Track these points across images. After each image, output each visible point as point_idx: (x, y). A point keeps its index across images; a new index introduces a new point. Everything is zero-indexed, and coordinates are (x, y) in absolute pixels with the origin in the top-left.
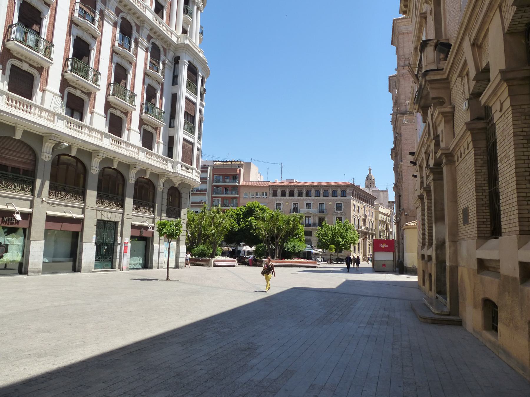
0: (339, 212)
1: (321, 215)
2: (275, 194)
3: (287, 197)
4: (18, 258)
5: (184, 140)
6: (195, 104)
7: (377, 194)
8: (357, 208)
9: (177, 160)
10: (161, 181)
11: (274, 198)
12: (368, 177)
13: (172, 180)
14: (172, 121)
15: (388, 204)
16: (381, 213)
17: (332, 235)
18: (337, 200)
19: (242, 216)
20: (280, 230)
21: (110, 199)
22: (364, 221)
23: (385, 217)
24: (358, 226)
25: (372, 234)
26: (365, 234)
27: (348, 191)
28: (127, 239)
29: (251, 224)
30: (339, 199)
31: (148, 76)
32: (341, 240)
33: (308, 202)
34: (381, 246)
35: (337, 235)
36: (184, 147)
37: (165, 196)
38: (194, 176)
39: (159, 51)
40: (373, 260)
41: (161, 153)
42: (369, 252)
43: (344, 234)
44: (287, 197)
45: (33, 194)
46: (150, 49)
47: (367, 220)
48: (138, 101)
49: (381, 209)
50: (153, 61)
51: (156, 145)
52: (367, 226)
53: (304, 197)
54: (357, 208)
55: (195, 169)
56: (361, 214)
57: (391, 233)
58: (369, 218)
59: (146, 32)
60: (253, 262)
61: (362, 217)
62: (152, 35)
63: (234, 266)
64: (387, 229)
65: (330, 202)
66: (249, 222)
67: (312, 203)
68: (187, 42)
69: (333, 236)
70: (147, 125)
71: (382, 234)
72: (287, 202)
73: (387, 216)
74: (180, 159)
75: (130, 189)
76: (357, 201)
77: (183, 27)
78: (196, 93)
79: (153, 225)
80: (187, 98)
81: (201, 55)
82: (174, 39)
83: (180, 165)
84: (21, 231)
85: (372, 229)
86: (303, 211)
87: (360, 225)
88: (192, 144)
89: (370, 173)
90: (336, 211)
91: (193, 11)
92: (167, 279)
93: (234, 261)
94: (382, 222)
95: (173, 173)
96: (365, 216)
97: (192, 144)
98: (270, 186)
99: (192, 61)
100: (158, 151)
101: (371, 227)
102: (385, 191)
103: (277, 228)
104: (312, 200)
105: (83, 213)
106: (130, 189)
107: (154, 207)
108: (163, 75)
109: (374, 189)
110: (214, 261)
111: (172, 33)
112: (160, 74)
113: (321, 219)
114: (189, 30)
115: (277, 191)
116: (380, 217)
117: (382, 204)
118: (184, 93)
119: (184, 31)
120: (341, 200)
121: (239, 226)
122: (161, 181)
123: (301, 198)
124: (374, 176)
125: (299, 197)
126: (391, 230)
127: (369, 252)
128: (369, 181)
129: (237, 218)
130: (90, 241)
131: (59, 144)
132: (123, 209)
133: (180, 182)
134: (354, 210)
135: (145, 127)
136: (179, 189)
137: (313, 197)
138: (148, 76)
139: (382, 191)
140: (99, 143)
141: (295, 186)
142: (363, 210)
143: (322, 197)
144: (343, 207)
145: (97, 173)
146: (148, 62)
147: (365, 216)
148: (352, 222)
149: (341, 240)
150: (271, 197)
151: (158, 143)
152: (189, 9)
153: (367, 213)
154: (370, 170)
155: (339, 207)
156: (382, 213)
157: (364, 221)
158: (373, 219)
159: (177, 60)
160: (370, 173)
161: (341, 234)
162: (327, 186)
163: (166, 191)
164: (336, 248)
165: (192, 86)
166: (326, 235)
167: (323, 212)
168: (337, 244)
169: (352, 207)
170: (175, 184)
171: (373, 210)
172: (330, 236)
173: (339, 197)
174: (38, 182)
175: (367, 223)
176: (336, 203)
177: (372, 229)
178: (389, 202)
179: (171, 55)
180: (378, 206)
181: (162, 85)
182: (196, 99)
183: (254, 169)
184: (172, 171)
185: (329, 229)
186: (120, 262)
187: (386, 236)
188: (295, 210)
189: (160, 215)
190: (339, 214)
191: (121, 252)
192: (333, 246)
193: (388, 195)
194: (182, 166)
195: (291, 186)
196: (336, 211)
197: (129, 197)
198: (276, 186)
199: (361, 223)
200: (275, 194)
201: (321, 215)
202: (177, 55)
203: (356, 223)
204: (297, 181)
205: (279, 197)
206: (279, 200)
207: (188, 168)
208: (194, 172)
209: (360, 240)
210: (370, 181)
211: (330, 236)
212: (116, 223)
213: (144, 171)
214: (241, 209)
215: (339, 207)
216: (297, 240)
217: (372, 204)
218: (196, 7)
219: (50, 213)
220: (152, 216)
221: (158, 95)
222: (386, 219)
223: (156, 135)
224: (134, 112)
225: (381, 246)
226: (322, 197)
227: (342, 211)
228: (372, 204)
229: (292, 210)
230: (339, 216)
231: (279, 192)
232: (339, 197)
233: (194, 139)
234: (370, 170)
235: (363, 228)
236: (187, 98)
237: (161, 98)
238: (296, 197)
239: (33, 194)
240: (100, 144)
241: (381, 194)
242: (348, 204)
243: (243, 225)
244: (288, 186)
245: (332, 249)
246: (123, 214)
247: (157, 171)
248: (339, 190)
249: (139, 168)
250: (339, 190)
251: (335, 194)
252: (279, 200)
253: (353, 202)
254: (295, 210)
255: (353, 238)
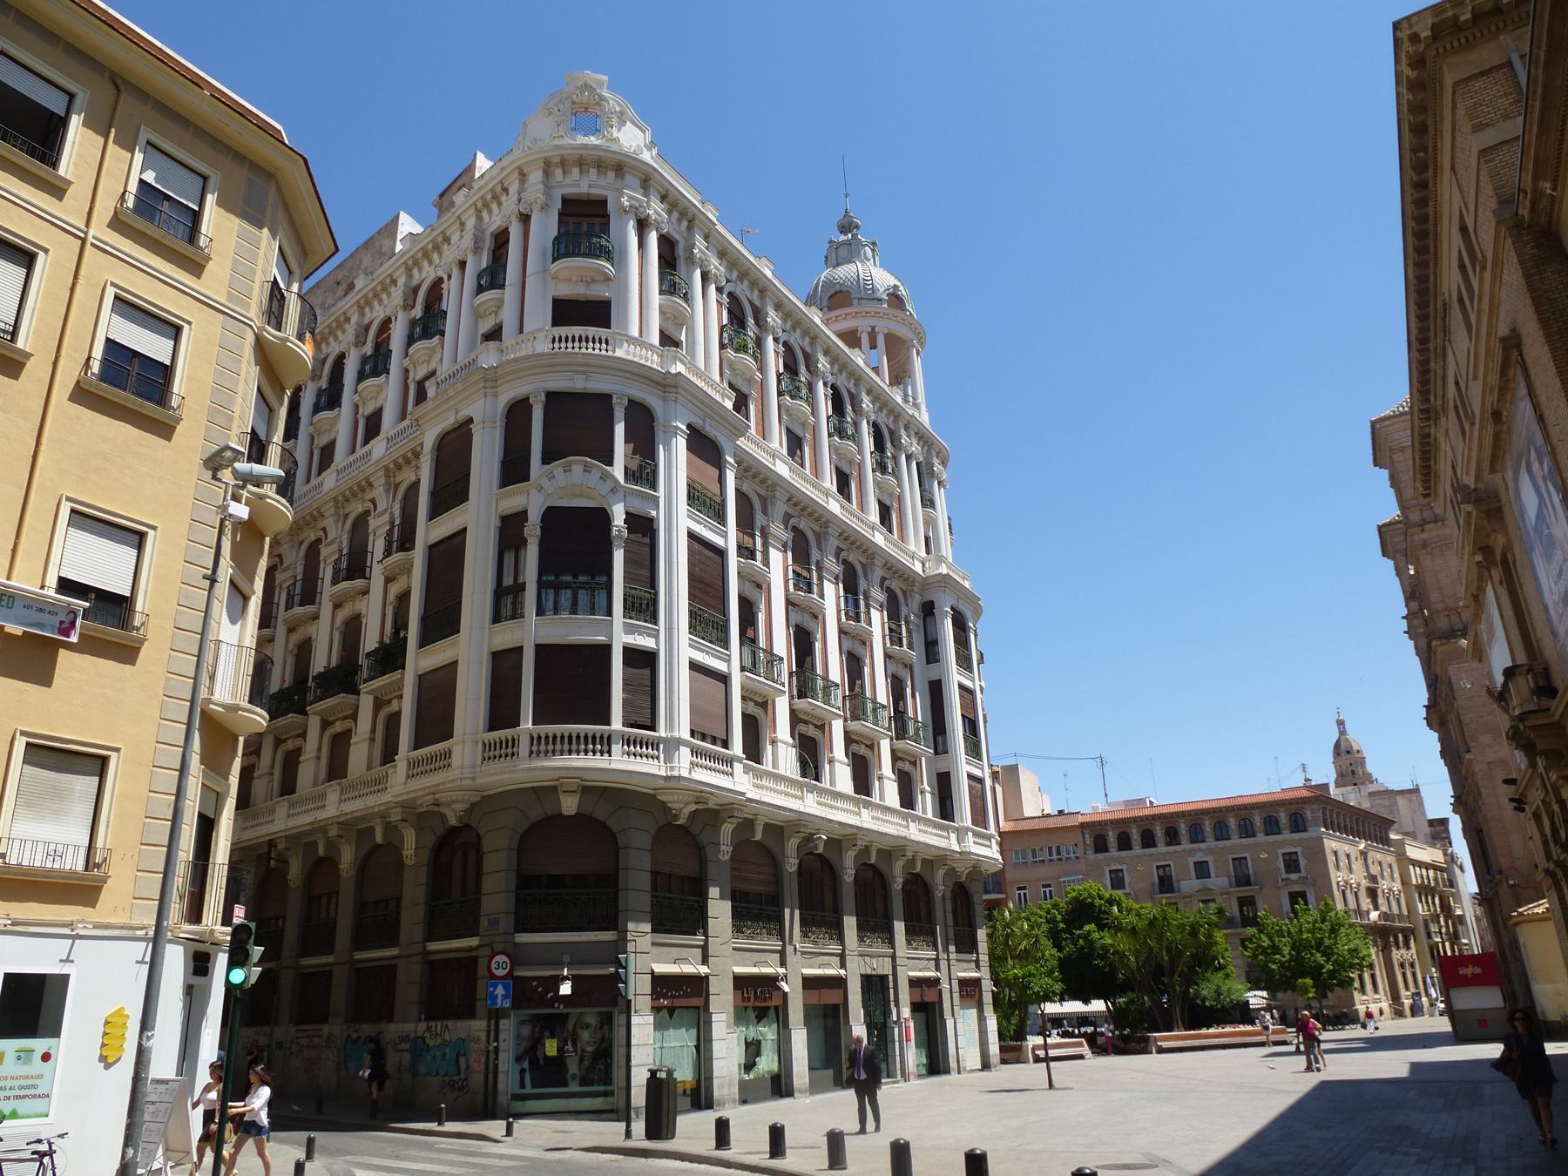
0: (1294, 876)
1: (1245, 891)
2: (1100, 846)
3: (1137, 850)
4: (775, 1067)
5: (695, 666)
6: (721, 553)
7: (1386, 802)
8: (1344, 862)
9: (676, 734)
10: (940, 874)
11: (1100, 856)
12: (1337, 745)
13: (664, 803)
14: (940, 739)
15: (1428, 830)
16: (1416, 863)
17: (1293, 947)
18: (1281, 844)
19: (1062, 925)
20: (1175, 954)
21: (757, 918)
22: (1372, 893)
23: (1431, 873)
24: (1359, 912)
25: (1403, 930)
26: (1385, 935)
27: (1308, 814)
28: (906, 1012)
29: (1090, 943)
30: (1287, 840)
31: (794, 605)
32: (1322, 960)
33: (1200, 857)
34: (1462, 971)
35: (1306, 946)
36: (971, 788)
37: (949, 907)
38: (990, 852)
39: (751, 507)
40: (1450, 1012)
41: (930, 815)
42: (1407, 989)
43: (1327, 942)
44: (1137, 850)
45: (783, 939)
46: (790, 544)
47: (1379, 892)
48: (837, 697)
49: (1414, 852)
50: (799, 570)
51: (769, 748)
52: (1384, 908)
53: (1186, 845)
54: (1344, 862)
55: (740, 760)
56: (1358, 877)
57: (1461, 919)
58: (1384, 885)
59: (780, 508)
60: (1120, 1044)
61: (1365, 883)
62: (791, 512)
63: (1081, 1057)
64: (1447, 909)
65: (1264, 851)
66: (1086, 937)
67: (1209, 859)
68: (679, 368)
69: (1299, 953)
70: (806, 722)
71: (1434, 928)
72: (1140, 865)
73: (1436, 868)
74: (969, 823)
75: (848, 898)
76: (1339, 839)
77: (661, 332)
78: (721, 517)
79: (842, 972)
80: (692, 536)
81: (967, 584)
82: (918, 568)
83: (685, 752)
84: (772, 1013)
85: (1400, 916)
86: (1189, 884)
87: (1364, 908)
88: (724, 679)
89: (1342, 733)
90: (1285, 876)
91: (689, 284)
92: (1051, 1086)
93: (1080, 1044)
94: (1425, 890)
95: (667, 778)
96: (1373, 879)
97: (724, 679)
98: (1083, 826)
99: (698, 423)
100: (924, 811)
101: (1396, 911)
102: (1410, 791)
103: (1169, 950)
104: (1210, 851)
105: (843, 965)
106: (848, 898)
107: (933, 934)
108: (910, 646)
109: (1372, 788)
110: (1033, 1049)
111: (774, 457)
112: (758, 563)
113: (1247, 902)
114: (683, 338)
115: (1105, 836)
116: (1415, 875)
117: (1413, 835)
118: (955, 677)
119: (668, 340)
120: (1293, 843)
121: (1060, 950)
122: (940, 874)
123: (1177, 848)
124: (1357, 738)
125: (1171, 848)
126: (1458, 912)
127: (1407, 989)
128: (1344, 756)
129: (1050, 931)
130: (858, 1020)
131: (809, 839)
132: (893, 947)
133: (693, 807)
134: (1338, 867)
135: (802, 728)
136: (695, 830)
137: (1211, 843)
138: (794, 605)
139: (1402, 792)
140: (903, 832)
141: (1155, 817)
142: (1361, 862)
143: (1236, 840)
144: (1302, 862)
145: (794, 869)
146: (791, 575)
147: (1373, 879)
148: (1340, 906)
149: (1322, 960)
150: (1092, 856)
151: (922, 792)
152: (677, 280)
153: (1375, 870)
154: (1341, 723)
155: (1292, 864)
156: (1421, 864)
157: (1372, 893)
158: (1397, 886)
159: (928, 609)
160: (1342, 733)
161: (1320, 942)
162: (1245, 807)
163: (949, 896)
164: (1310, 988)
165: (964, 661)
166: (1276, 949)
167: (1248, 883)
168: (1316, 972)
169: (1331, 859)
170: (676, 817)
171: (1390, 859)
172: (1286, 950)
173: (1286, 835)
174: (787, 912)
175: (1381, 900)
176: (1280, 851)
177: (1400, 916)
178: (1431, 823)
179: (916, 601)
180: (1401, 844)
181: (911, 668)
182: (725, 535)
183: (1028, 781)
184: (957, 849)
185: (1280, 933)
186: (902, 1062)
187: (1448, 932)
188: (1166, 883)
189: (946, 950)
190: (1294, 882)
191: (901, 1042)
192: (1309, 981)
193: (1421, 803)
194: (695, 751)
195: (1142, 819)
196: (1285, 876)
197: (850, 914)
198: (1099, 823)
199: (1366, 903)
200: (1100, 846)
201: (1245, 891)
202: (928, 598)
203: (1352, 905)
204: (1156, 803)
205: (1114, 852)
206: (1115, 860)
207: (716, 758)
208: (738, 767)
209: (1374, 954)
210: (1349, 761)
211: (1286, 950)
212: (884, 978)
213: (866, 850)
214: (1055, 906)
215: (1292, 864)
216: (1220, 974)
217: (1386, 841)
218: (698, 272)
219: (739, 970)
220: (932, 954)
221: (909, 691)
222: (1436, 879)
223: (915, 775)
224: (778, 700)
225: (1462, 971)
226: (1236, 840)
227: (1303, 874)
228: (1386, 841)
229: (1157, 887)
230: (1297, 888)
231: (1112, 838)
232: (1286, 835)
233: (728, 661)
234: (1341, 723)
235: (1374, 915)
236: (692, 536)
237: (913, 696)
238: (1161, 848)
239: (783, 939)
240: (858, 824)
241: (1400, 801)
242: (1318, 853)
243: (1069, 948)
244: (1135, 820)
245: (1307, 992)
246: (894, 957)
247: (837, 833)
248: (1282, 815)
249: (861, 844)
250: (1282, 815)
251: (1272, 826)
252: (1115, 860)
253: (1330, 844)
254: (1166, 883)
255: (1355, 950)
